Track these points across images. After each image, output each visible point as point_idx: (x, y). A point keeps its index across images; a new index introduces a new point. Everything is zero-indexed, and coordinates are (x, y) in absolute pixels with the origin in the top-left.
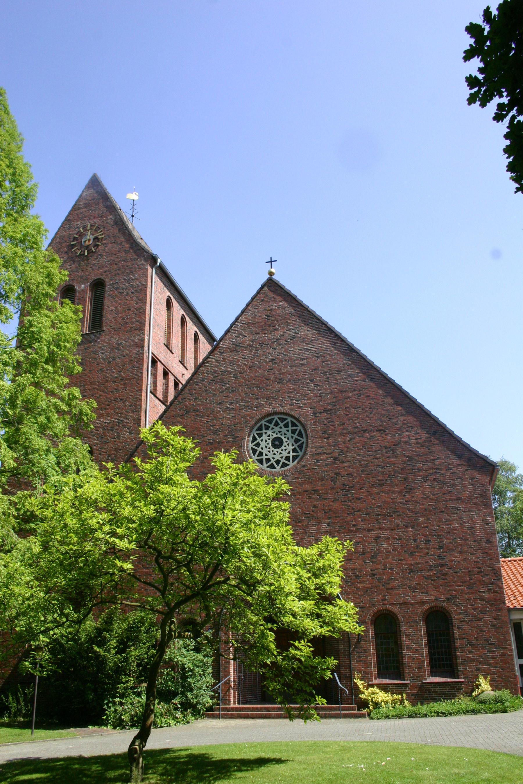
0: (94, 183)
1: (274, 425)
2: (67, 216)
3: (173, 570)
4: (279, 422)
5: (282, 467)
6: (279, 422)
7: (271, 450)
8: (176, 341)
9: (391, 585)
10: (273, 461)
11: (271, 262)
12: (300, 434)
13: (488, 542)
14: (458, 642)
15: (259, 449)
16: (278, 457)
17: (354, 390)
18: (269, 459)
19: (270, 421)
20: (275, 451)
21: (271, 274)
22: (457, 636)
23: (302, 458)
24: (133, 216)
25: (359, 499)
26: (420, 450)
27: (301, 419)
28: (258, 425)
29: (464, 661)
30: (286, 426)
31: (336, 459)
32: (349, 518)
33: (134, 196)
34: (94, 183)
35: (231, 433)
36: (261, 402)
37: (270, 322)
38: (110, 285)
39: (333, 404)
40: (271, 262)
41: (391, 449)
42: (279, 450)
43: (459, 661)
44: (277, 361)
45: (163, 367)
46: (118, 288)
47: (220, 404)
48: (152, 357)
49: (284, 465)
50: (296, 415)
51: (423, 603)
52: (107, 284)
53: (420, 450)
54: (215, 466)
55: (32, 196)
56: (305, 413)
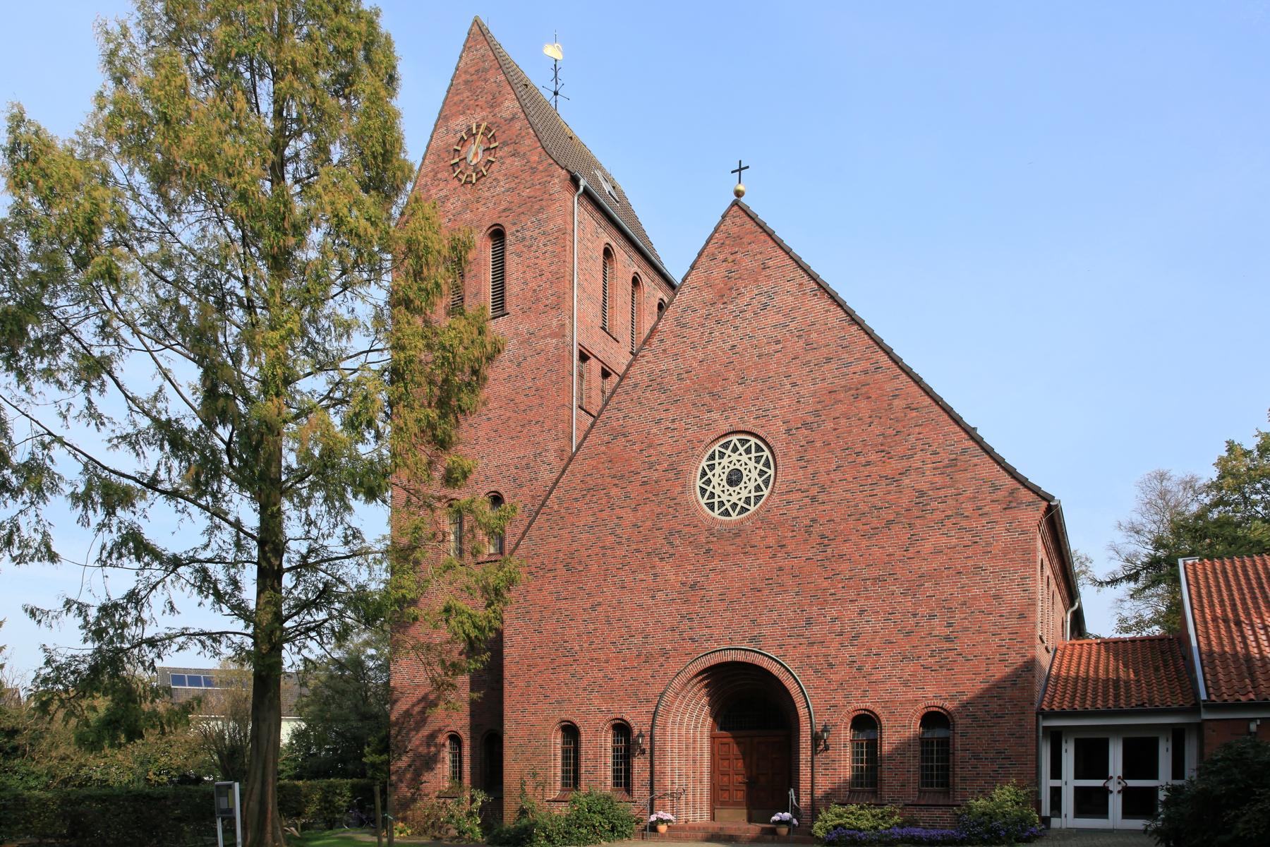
0: (479, 33)
2: (441, 111)
4: (739, 445)
5: (739, 513)
6: (739, 445)
9: (874, 678)
10: (728, 505)
11: (740, 170)
12: (767, 464)
13: (1022, 616)
14: (959, 754)
15: (710, 489)
16: (734, 499)
17: (850, 389)
19: (726, 446)
21: (739, 194)
23: (767, 499)
24: (556, 93)
25: (841, 556)
29: (964, 779)
31: (813, 499)
32: (825, 584)
33: (552, 51)
34: (479, 33)
35: (671, 467)
36: (715, 415)
38: (513, 234)
39: (816, 413)
40: (740, 170)
42: (737, 489)
43: (957, 780)
44: (739, 349)
46: (524, 239)
49: (744, 510)
50: (762, 434)
52: (508, 233)
53: (939, 480)
54: (378, 280)
56: (775, 431)
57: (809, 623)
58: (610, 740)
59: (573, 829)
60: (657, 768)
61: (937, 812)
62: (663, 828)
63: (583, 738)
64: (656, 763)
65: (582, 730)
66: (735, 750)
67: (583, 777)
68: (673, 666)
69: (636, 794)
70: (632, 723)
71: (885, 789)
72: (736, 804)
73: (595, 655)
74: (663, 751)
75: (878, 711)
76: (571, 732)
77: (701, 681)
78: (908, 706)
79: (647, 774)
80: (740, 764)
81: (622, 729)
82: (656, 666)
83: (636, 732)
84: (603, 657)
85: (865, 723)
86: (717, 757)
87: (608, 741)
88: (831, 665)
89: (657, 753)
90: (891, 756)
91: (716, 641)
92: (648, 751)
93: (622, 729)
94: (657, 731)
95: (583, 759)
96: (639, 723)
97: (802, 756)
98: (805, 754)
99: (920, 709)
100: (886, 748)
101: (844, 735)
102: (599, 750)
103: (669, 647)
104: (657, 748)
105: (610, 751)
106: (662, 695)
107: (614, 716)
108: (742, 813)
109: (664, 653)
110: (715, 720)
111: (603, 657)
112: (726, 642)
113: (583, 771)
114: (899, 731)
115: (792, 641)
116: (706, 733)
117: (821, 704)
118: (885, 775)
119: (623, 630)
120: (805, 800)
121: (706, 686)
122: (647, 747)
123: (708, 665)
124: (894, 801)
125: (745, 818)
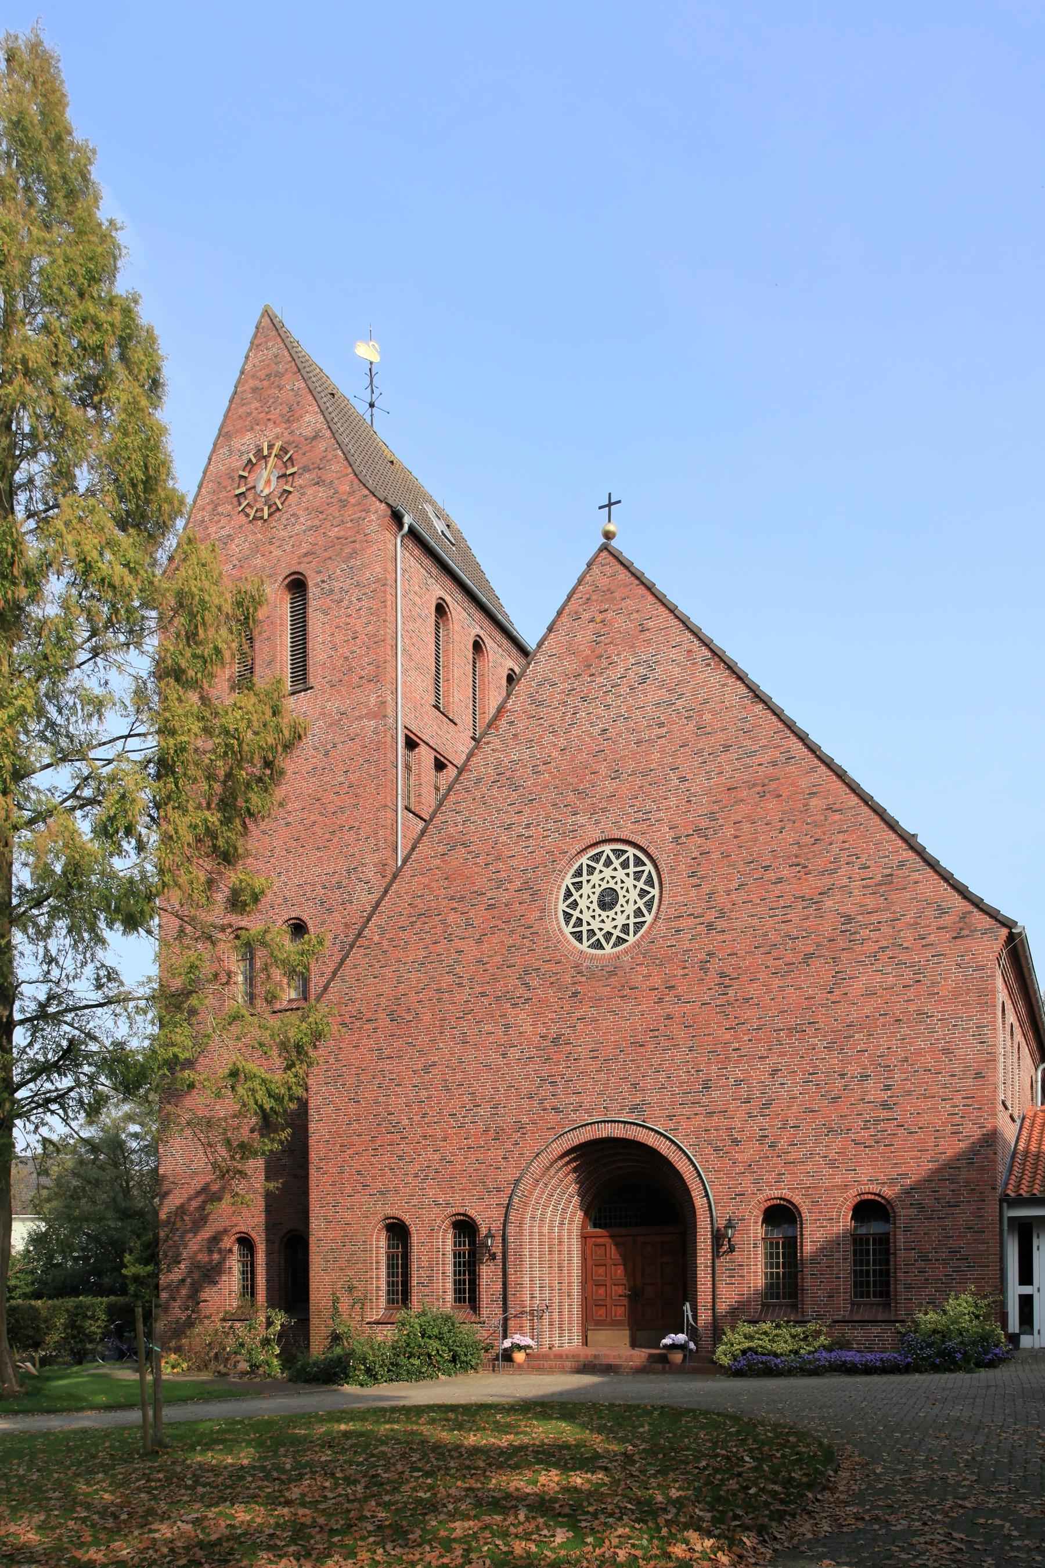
1: (604, 865)
3: (717, 1455)
5: (615, 945)
6: (613, 857)
7: (596, 914)
8: (459, 698)
9: (791, 1157)
10: (599, 935)
11: (610, 505)
12: (650, 882)
16: (608, 927)
17: (754, 785)
18: (592, 930)
20: (604, 914)
21: (608, 535)
22: (901, 1244)
26: (871, 902)
27: (651, 850)
28: (576, 866)
29: (909, 1287)
30: (608, 863)
31: (710, 926)
35: (526, 886)
36: (581, 819)
37: (599, 650)
38: (317, 585)
39: (712, 816)
40: (610, 505)
41: (814, 902)
42: (611, 913)
43: (900, 1288)
45: (434, 753)
46: (332, 591)
47: (509, 827)
48: (407, 736)
49: (620, 941)
51: (846, 1187)
53: (871, 902)
55: (163, 463)
58: (450, 1241)
59: (402, 1360)
60: (511, 1278)
61: (875, 1330)
62: (519, 1357)
63: (415, 1239)
64: (511, 1271)
65: (413, 1229)
66: (613, 1253)
69: (484, 1312)
70: (479, 1219)
71: (808, 1300)
72: (615, 1324)
74: (520, 1257)
75: (797, 1200)
76: (398, 1232)
78: (836, 1193)
81: (465, 1227)
82: (509, 1145)
83: (484, 1231)
86: (590, 1263)
87: (447, 1243)
88: (736, 1142)
89: (511, 1258)
90: (814, 1259)
91: (587, 1111)
92: (499, 1256)
93: (465, 1227)
94: (511, 1230)
96: (487, 1219)
97: (700, 1260)
99: (851, 1197)
100: (808, 1249)
103: (525, 1120)
104: (511, 1252)
107: (454, 1210)
109: (520, 1127)
111: (440, 1134)
117: (724, 1193)
118: (808, 1283)
121: (575, 1170)
122: (498, 1250)
123: (576, 1142)
124: (819, 1317)
125: (627, 1341)
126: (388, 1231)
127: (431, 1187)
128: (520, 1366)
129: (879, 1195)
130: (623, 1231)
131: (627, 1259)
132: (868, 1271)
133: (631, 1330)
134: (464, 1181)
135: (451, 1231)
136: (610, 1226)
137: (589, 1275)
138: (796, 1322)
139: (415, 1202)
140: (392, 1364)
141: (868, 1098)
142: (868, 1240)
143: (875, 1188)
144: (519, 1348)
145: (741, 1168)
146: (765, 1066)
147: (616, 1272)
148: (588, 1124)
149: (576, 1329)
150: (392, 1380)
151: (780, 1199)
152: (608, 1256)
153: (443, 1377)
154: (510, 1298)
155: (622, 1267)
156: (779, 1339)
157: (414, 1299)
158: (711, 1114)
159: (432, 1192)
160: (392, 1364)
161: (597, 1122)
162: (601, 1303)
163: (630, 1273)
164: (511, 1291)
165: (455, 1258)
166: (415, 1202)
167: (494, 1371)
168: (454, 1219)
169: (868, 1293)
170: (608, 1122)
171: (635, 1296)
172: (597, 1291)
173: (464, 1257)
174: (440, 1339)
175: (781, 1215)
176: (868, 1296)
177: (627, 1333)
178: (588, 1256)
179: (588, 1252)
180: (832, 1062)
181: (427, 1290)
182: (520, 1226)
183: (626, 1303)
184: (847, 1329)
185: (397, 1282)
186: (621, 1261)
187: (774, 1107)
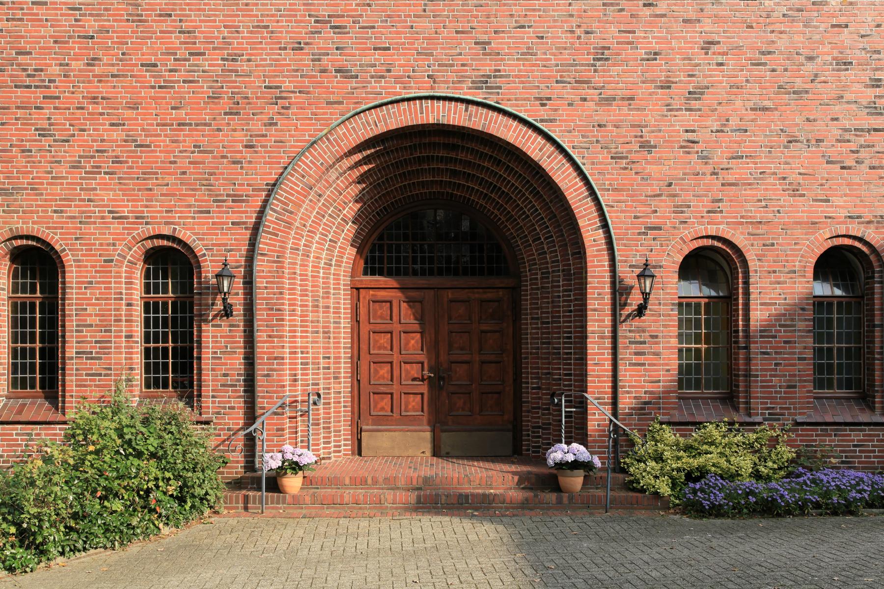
9: (730, 178)
57: (602, 55)
58: (138, 282)
59: (93, 506)
60: (262, 348)
61: (856, 436)
62: (293, 483)
63: (72, 276)
64: (260, 336)
65: (69, 259)
66: (405, 314)
67: (72, 366)
68: (295, 132)
69: (209, 403)
70: (199, 247)
71: (757, 391)
72: (407, 421)
73: (103, 90)
74: (276, 311)
75: (739, 240)
76: (37, 263)
77: (366, 160)
78: (798, 232)
79: (238, 362)
80: (415, 340)
81: (170, 261)
82: (257, 126)
83: (209, 269)
84: (123, 96)
85: (714, 264)
86: (365, 328)
87: (131, 284)
88: (646, 146)
89: (261, 315)
90: (765, 332)
91: (398, 79)
92: (239, 309)
93: (170, 261)
94: (261, 265)
95: (71, 324)
96: (215, 247)
97: (592, 327)
98: (598, 322)
99: (819, 243)
100: (759, 315)
101: (671, 289)
102: (106, 311)
103: (287, 85)
104: (260, 305)
105: (138, 311)
106: (273, 187)
107: (151, 230)
108: (420, 440)
109: (278, 97)
110: (360, 252)
111: (123, 96)
112: (425, 77)
113: (71, 351)
114: (780, 287)
115: (568, 93)
116: (345, 280)
117: (635, 220)
118: (757, 365)
119: (175, 40)
120: (598, 417)
121: (361, 180)
122: (237, 301)
123: (382, 129)
124: (773, 417)
125: (427, 447)
126: (13, 260)
127: (105, 186)
128: (296, 501)
129: (860, 239)
130: (411, 281)
131: (429, 321)
132: (830, 350)
133: (433, 431)
134: (171, 179)
135: (140, 265)
136: (406, 274)
137: (364, 347)
138: (741, 424)
139: (73, 211)
140: (75, 516)
141: (848, 96)
142: (830, 305)
143: (856, 229)
144: (296, 467)
145: (656, 187)
146: (694, 36)
147: (407, 344)
148: (403, 100)
149: (345, 428)
150: (74, 550)
151: (713, 238)
152: (395, 318)
153: (165, 530)
154: (260, 381)
155: (419, 335)
156: (727, 451)
157: (71, 380)
158: (610, 100)
159: (107, 196)
160: (75, 516)
161: (420, 98)
162: (383, 389)
163: (432, 346)
164: (260, 370)
165: (147, 311)
166: (73, 211)
167: (246, 508)
168: (149, 244)
169: (830, 381)
170: (439, 98)
171: (438, 381)
172: (376, 371)
173: (165, 311)
174: (159, 459)
175: (714, 264)
176: (830, 387)
177: (428, 435)
178: (363, 317)
179: (363, 311)
180: (796, 38)
181: (96, 366)
182: (279, 262)
183: (424, 389)
184: (815, 436)
185: (33, 350)
186: (417, 327)
187: (709, 99)
